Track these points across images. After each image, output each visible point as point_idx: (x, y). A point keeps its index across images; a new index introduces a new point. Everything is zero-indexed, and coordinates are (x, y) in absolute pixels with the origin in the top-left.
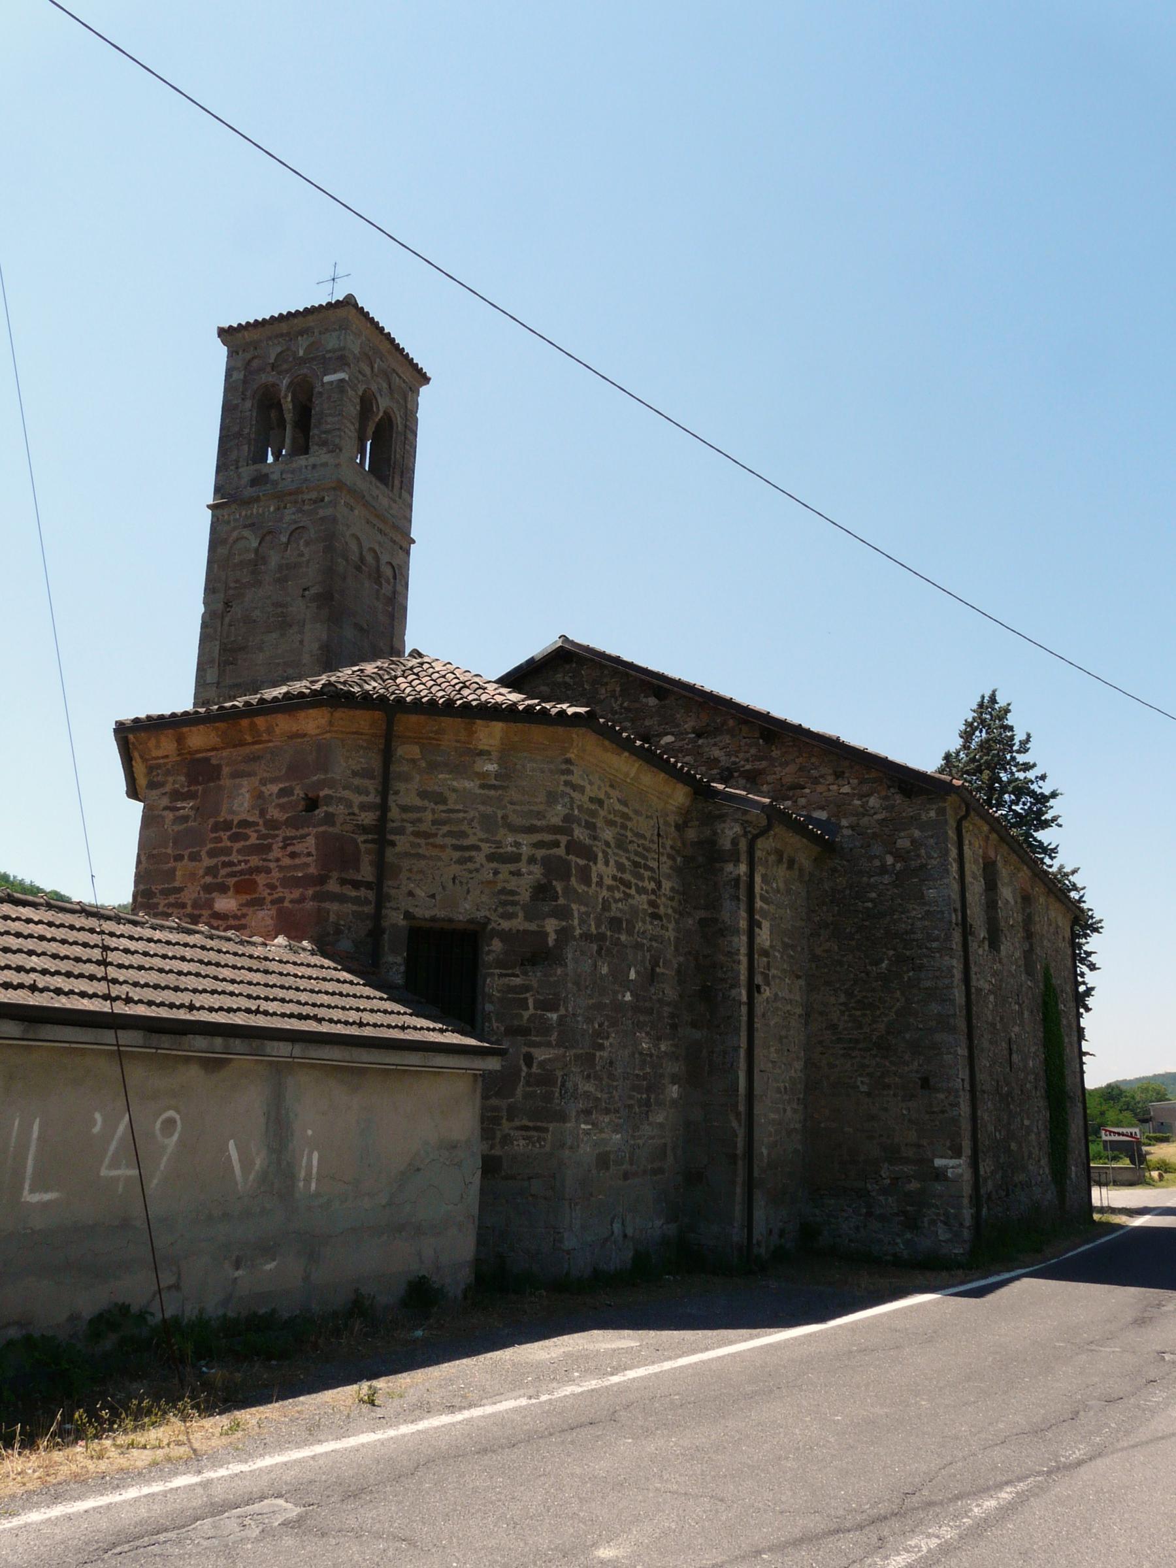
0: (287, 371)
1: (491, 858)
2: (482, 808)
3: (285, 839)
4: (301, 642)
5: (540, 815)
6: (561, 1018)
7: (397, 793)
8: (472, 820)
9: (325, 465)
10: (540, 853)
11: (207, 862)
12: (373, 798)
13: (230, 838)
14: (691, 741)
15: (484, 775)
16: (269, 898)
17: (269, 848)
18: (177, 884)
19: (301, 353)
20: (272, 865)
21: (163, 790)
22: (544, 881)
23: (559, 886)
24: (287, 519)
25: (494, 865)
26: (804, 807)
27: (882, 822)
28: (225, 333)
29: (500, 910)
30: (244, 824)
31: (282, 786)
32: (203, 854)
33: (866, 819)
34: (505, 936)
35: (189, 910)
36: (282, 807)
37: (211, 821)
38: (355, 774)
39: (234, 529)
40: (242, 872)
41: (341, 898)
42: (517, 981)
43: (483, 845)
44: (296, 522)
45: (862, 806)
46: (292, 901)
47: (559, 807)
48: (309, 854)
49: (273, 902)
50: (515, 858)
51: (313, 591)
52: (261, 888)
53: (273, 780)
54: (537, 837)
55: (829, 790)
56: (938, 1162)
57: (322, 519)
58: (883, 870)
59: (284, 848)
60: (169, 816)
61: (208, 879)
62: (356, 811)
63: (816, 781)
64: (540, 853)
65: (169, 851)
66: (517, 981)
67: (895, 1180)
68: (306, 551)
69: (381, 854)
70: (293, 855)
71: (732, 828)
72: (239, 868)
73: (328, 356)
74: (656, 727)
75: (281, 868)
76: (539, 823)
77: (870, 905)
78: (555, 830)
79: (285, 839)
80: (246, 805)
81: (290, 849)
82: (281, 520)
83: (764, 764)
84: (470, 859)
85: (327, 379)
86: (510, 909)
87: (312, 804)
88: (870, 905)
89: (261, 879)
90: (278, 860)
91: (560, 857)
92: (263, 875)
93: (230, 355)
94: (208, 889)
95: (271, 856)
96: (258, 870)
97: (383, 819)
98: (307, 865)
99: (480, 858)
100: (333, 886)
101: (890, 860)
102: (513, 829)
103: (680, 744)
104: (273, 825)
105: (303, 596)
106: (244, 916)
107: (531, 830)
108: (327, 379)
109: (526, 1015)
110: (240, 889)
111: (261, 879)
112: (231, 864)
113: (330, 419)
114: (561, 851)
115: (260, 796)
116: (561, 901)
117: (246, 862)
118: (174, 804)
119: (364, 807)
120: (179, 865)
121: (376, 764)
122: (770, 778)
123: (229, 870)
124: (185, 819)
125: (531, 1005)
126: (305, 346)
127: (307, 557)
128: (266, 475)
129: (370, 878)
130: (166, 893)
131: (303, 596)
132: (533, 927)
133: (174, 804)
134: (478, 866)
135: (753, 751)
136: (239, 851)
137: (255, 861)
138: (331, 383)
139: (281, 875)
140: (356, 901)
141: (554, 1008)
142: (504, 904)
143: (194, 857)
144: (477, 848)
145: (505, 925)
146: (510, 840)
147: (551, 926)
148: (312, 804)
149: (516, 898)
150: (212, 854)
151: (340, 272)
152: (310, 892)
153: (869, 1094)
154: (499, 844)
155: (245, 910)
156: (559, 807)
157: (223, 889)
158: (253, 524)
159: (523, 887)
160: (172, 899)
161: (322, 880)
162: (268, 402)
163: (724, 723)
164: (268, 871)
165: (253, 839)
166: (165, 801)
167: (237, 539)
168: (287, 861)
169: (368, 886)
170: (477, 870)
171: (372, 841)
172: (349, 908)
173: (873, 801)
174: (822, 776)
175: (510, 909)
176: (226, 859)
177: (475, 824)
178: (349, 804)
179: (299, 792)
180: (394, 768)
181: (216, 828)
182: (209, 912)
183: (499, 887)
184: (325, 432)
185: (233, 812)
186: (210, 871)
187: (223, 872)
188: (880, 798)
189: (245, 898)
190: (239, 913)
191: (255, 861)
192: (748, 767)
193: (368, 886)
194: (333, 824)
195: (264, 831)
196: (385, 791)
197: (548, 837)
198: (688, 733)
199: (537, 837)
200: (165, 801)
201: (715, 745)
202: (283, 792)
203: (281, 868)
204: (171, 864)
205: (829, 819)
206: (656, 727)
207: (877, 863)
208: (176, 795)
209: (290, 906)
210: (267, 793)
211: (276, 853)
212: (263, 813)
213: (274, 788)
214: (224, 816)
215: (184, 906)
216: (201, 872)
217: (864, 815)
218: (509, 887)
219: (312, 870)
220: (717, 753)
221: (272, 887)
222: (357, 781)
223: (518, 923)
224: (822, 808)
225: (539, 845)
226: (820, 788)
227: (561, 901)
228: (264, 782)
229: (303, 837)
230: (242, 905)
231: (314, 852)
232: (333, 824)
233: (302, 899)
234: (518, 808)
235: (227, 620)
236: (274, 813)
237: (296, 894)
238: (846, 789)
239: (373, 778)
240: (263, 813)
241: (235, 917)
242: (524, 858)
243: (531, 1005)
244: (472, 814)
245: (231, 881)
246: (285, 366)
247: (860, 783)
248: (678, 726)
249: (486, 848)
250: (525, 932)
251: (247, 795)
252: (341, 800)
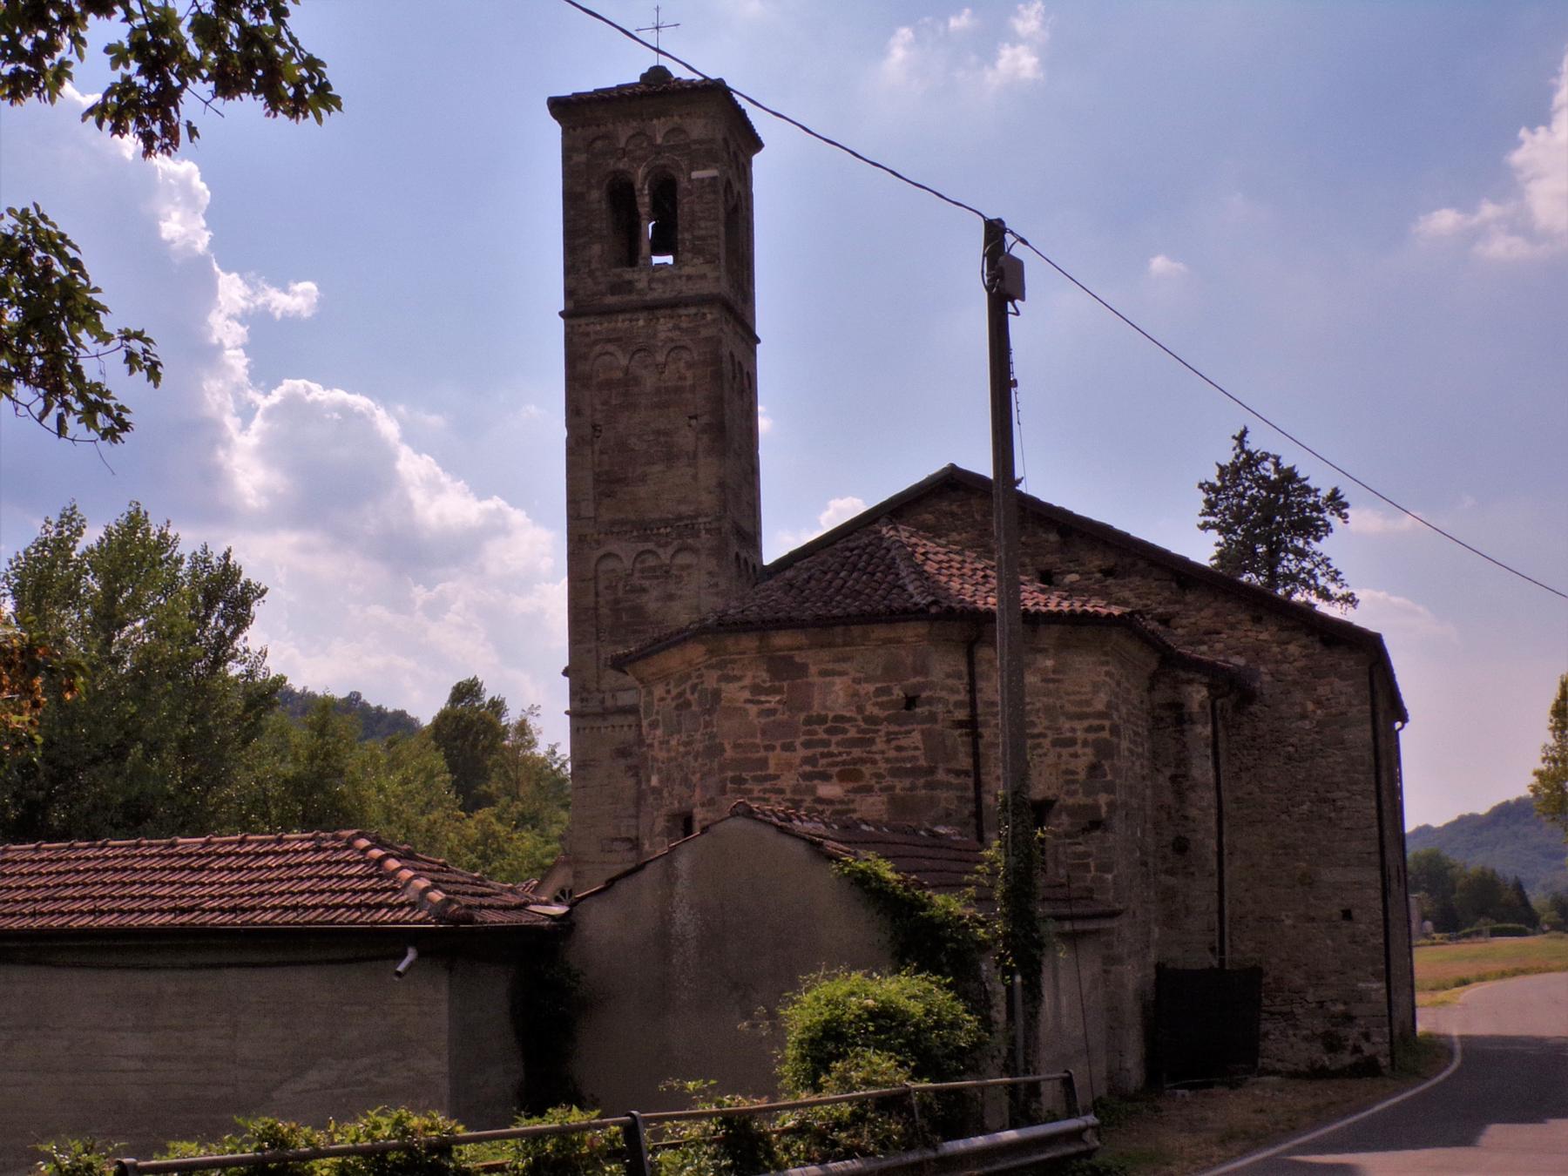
0: (644, 159)
1: (1055, 743)
3: (888, 734)
4: (695, 477)
5: (1088, 703)
9: (703, 277)
10: (1091, 736)
11: (802, 752)
12: (963, 696)
13: (828, 731)
14: (1098, 581)
16: (877, 786)
17: (872, 741)
18: (771, 771)
19: (659, 141)
20: (878, 757)
24: (662, 336)
26: (1220, 652)
27: (1302, 671)
28: (561, 107)
32: (798, 743)
33: (1286, 666)
35: (789, 795)
36: (881, 705)
38: (948, 676)
40: (844, 763)
41: (949, 786)
42: (1081, 848)
44: (672, 340)
48: (916, 748)
49: (881, 790)
50: (1072, 742)
53: (867, 680)
54: (1086, 723)
58: (1304, 716)
59: (888, 741)
60: (753, 709)
61: (808, 768)
63: (1233, 627)
64: (1091, 736)
65: (758, 741)
66: (1081, 848)
69: (975, 745)
70: (899, 749)
72: (839, 759)
73: (694, 147)
75: (887, 760)
79: (888, 734)
81: (894, 744)
82: (655, 336)
83: (1177, 607)
85: (695, 175)
86: (1073, 787)
87: (911, 702)
89: (867, 770)
90: (883, 752)
93: (564, 133)
94: (807, 777)
95: (874, 748)
96: (863, 761)
98: (914, 758)
99: (1046, 742)
101: (1310, 706)
107: (1081, 717)
108: (695, 175)
109: (1089, 876)
110: (844, 777)
111: (867, 770)
112: (831, 755)
113: (703, 224)
114: (1105, 734)
115: (856, 694)
116: (1109, 777)
119: (958, 705)
120: (771, 754)
121: (963, 668)
124: (772, 712)
126: (663, 132)
127: (689, 382)
128: (630, 282)
132: (1090, 801)
136: (838, 744)
137: (857, 752)
138: (702, 180)
141: (1109, 871)
142: (1068, 782)
143: (788, 747)
144: (1044, 736)
145: (1070, 801)
146: (1067, 726)
147: (1103, 799)
148: (911, 702)
150: (807, 745)
152: (922, 781)
154: (1059, 730)
155: (852, 796)
157: (825, 777)
159: (1081, 765)
162: (621, 194)
163: (1134, 565)
166: (747, 695)
168: (892, 754)
169: (966, 773)
171: (967, 735)
173: (1293, 649)
175: (1073, 787)
178: (946, 703)
179: (898, 693)
180: (978, 669)
181: (808, 721)
183: (1063, 767)
185: (825, 708)
186: (806, 761)
187: (823, 761)
189: (850, 785)
191: (857, 752)
193: (966, 773)
196: (972, 690)
197: (1096, 722)
199: (1086, 723)
200: (747, 695)
202: (878, 692)
203: (887, 760)
204: (762, 753)
207: (1298, 709)
210: (862, 692)
211: (880, 744)
212: (860, 709)
213: (871, 688)
214: (816, 709)
215: (781, 791)
216: (798, 761)
218: (1071, 767)
220: (1127, 594)
221: (878, 776)
222: (950, 682)
223: (1081, 799)
225: (1089, 729)
227: (1109, 777)
228: (857, 681)
236: (871, 709)
237: (907, 783)
239: (960, 678)
240: (860, 709)
241: (841, 802)
244: (1038, 705)
246: (639, 153)
252: (939, 700)
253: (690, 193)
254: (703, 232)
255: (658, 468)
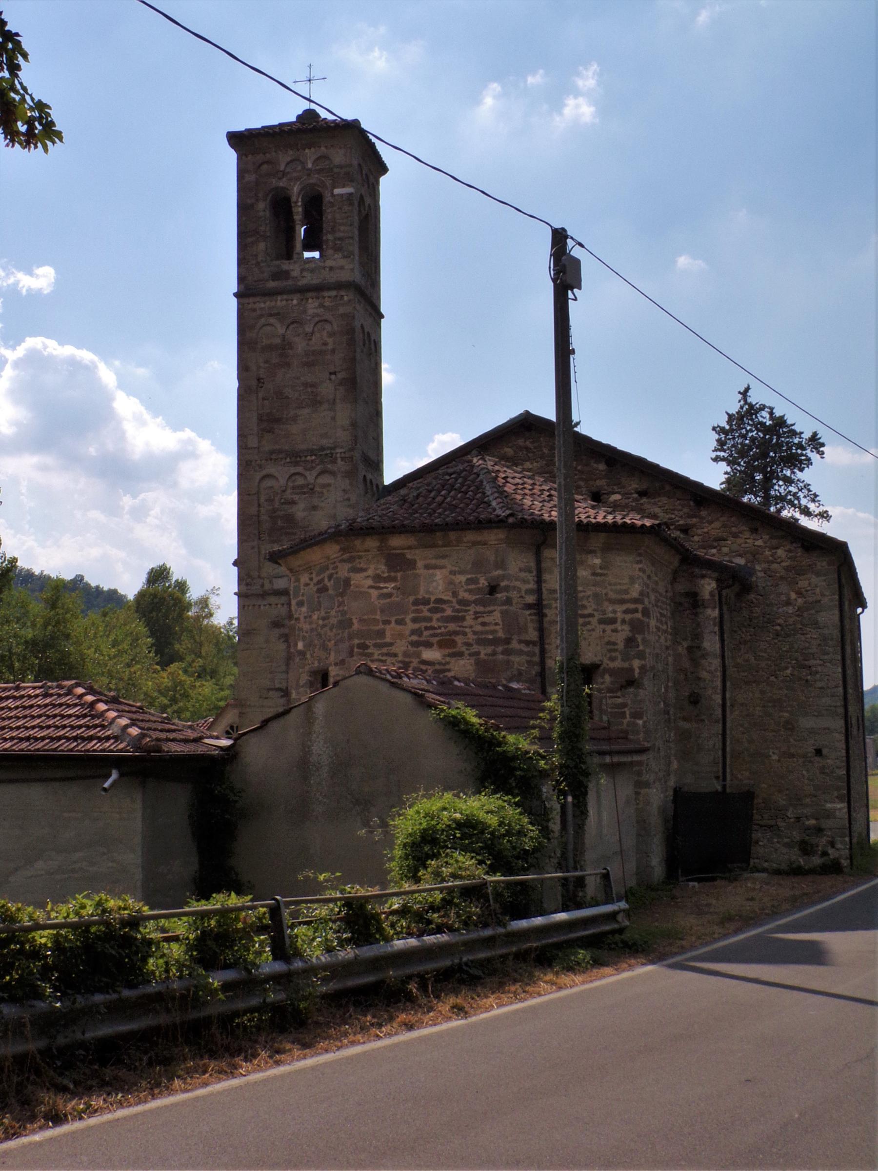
1: (601, 622)
2: (593, 588)
3: (476, 613)
4: (333, 418)
5: (626, 592)
6: (645, 722)
7: (545, 581)
8: (589, 597)
9: (342, 268)
10: (628, 617)
11: (411, 626)
12: (532, 586)
13: (429, 610)
14: (635, 500)
15: (593, 567)
16: (467, 652)
17: (463, 619)
20: (467, 630)
21: (365, 574)
22: (631, 635)
23: (639, 638)
24: (310, 312)
25: (602, 626)
26: (727, 554)
27: (787, 569)
28: (239, 140)
29: (608, 655)
30: (439, 601)
31: (469, 576)
32: (408, 620)
34: (612, 672)
35: (400, 658)
36: (470, 591)
37: (411, 599)
38: (521, 570)
39: (261, 316)
40: (441, 634)
41: (520, 653)
42: (620, 700)
43: (596, 613)
45: (772, 556)
46: (486, 655)
47: (637, 586)
48: (496, 624)
49: (470, 655)
50: (613, 621)
51: (340, 376)
52: (460, 645)
55: (746, 543)
56: (829, 806)
57: (342, 315)
58: (788, 603)
61: (415, 638)
62: (523, 594)
63: (735, 535)
64: (628, 617)
65: (378, 617)
66: (620, 700)
67: (798, 819)
68: (330, 341)
70: (484, 624)
71: (709, 584)
72: (439, 631)
73: (336, 170)
74: (606, 487)
75: (475, 633)
76: (624, 596)
77: (778, 628)
78: (635, 601)
79: (476, 613)
80: (440, 588)
81: (480, 620)
82: (305, 312)
84: (589, 623)
85: (337, 191)
86: (614, 654)
87: (493, 589)
88: (778, 628)
89: (459, 639)
90: (471, 627)
91: (638, 619)
92: (461, 636)
95: (465, 624)
96: (456, 633)
97: (540, 600)
99: (594, 621)
100: (515, 645)
101: (793, 596)
102: (612, 602)
103: (627, 501)
104: (463, 602)
105: (330, 379)
106: (448, 663)
107: (622, 602)
108: (337, 191)
109: (625, 721)
110: (441, 645)
113: (342, 228)
116: (641, 648)
117: (446, 627)
118: (378, 585)
119: (529, 592)
120: (387, 627)
121: (533, 564)
122: (699, 532)
123: (431, 632)
124: (389, 595)
125: (628, 716)
127: (330, 347)
129: (536, 639)
130: (378, 646)
131: (330, 379)
132: (626, 665)
133: (378, 585)
134: (593, 627)
135: (686, 510)
136: (438, 620)
137: (452, 627)
138: (342, 195)
139: (475, 637)
140: (527, 654)
141: (641, 718)
142: (610, 651)
145: (612, 665)
146: (610, 609)
147: (636, 663)
148: (493, 589)
149: (616, 647)
150: (414, 620)
151: (315, 74)
153: (779, 761)
155: (448, 659)
156: (637, 586)
157: (428, 645)
158: (278, 314)
159: (620, 639)
160: (385, 650)
161: (508, 641)
162: (281, 205)
164: (465, 634)
165: (449, 612)
166: (370, 582)
167: (264, 325)
168: (479, 628)
169: (534, 643)
170: (593, 630)
171: (535, 614)
172: (524, 658)
173: (780, 552)
174: (741, 533)
175: (614, 654)
176: (429, 625)
177: (590, 600)
179: (483, 582)
180: (543, 565)
181: (416, 603)
182: (418, 660)
183: (606, 639)
184: (340, 239)
188: (786, 551)
189: (447, 651)
190: (443, 661)
191: (452, 627)
192: (681, 522)
193: (534, 643)
194: (511, 605)
195: (458, 607)
196: (539, 581)
197: (632, 606)
198: (631, 494)
200: (370, 582)
201: (655, 504)
202: (470, 581)
203: (475, 633)
205: (746, 565)
206: (606, 487)
208: (378, 578)
209: (486, 658)
213: (463, 578)
214: (422, 594)
215: (395, 655)
216: (407, 633)
217: (773, 562)
219: (501, 634)
220: (657, 510)
221: (468, 645)
222: (523, 575)
223: (618, 664)
224: (741, 556)
226: (739, 541)
227: (641, 648)
229: (492, 612)
230: (445, 656)
231: (500, 622)
232: (511, 605)
233: (494, 654)
234: (614, 587)
235: (260, 395)
236: (463, 595)
238: (759, 543)
239: (531, 572)
240: (455, 594)
241: (440, 663)
242: (619, 620)
243: (628, 716)
244: (589, 593)
245: (434, 640)
247: (771, 538)
248: (624, 487)
249: (597, 616)
250: (623, 669)
251: (441, 582)
252: (514, 588)
253: (332, 205)
254: (341, 235)
255: (306, 411)
